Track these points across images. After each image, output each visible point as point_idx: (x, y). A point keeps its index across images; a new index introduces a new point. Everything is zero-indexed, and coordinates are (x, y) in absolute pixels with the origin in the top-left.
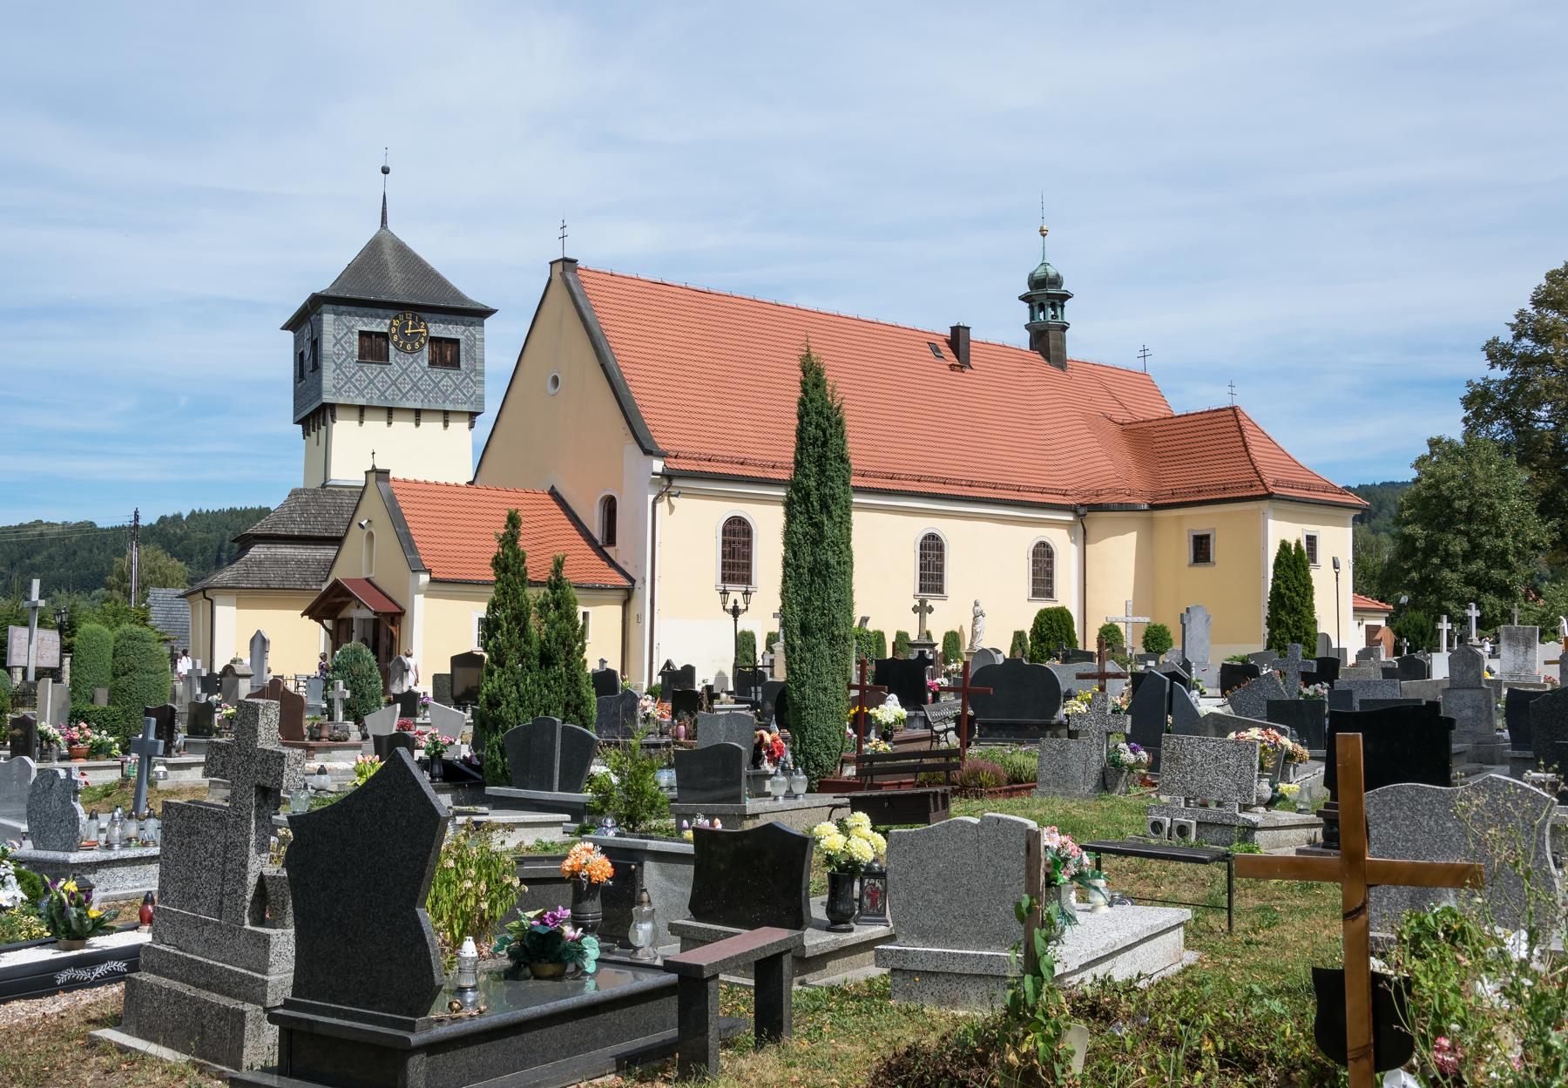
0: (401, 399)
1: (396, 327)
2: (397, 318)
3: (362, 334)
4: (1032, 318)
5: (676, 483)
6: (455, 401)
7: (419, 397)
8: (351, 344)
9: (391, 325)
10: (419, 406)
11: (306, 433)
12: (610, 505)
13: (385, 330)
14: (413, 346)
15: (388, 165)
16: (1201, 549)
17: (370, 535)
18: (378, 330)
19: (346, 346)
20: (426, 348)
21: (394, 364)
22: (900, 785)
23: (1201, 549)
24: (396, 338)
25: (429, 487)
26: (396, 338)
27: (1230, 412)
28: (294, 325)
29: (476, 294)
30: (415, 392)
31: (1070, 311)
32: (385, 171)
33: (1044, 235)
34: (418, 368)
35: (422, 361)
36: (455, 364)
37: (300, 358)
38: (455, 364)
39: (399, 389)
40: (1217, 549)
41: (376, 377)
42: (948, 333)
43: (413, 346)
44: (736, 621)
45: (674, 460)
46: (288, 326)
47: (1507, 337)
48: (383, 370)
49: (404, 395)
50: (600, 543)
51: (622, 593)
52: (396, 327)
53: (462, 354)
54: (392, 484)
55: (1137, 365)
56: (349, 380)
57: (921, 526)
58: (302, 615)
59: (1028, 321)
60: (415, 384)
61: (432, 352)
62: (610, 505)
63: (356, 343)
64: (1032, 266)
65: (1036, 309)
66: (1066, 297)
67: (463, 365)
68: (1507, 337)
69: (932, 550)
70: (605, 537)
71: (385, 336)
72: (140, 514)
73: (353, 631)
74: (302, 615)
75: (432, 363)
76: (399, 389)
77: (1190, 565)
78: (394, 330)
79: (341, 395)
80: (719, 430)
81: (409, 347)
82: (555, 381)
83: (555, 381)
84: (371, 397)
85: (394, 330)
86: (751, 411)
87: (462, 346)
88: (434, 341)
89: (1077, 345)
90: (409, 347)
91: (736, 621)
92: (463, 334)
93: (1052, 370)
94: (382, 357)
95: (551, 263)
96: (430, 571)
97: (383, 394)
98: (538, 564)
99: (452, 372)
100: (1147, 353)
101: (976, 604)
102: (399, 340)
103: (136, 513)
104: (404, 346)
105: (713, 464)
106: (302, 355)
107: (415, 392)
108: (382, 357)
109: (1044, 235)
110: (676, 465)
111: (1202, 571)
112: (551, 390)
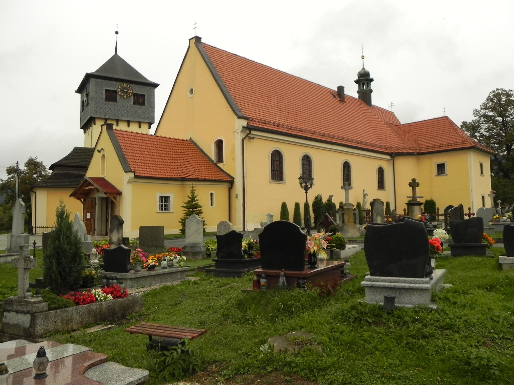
0: (122, 116)
1: (120, 89)
2: (121, 85)
3: (106, 90)
4: (359, 88)
5: (253, 132)
6: (143, 118)
7: (129, 116)
8: (102, 94)
9: (118, 88)
10: (129, 120)
11: (85, 132)
12: (219, 144)
13: (116, 90)
14: (127, 96)
15: (118, 31)
16: (441, 168)
17: (104, 156)
18: (113, 89)
19: (100, 95)
20: (132, 97)
21: (119, 103)
22: (410, 283)
23: (441, 168)
24: (120, 92)
25: (133, 134)
26: (120, 93)
27: (445, 118)
28: (80, 90)
29: (151, 78)
30: (128, 114)
31: (373, 85)
32: (117, 33)
33: (363, 59)
34: (129, 105)
35: (131, 102)
36: (143, 104)
37: (82, 102)
38: (143, 104)
39: (121, 113)
40: (448, 169)
41: (112, 107)
42: (336, 89)
43: (127, 96)
44: (306, 193)
45: (251, 122)
46: (78, 91)
47: (479, 108)
48: (115, 105)
49: (123, 115)
50: (215, 162)
51: (227, 184)
52: (120, 89)
53: (146, 100)
54: (115, 131)
55: (389, 109)
56: (101, 108)
57: (344, 158)
58: (70, 196)
59: (358, 90)
60: (128, 111)
61: (134, 99)
62: (219, 144)
63: (104, 94)
64: (359, 69)
65: (361, 85)
66: (372, 80)
67: (146, 105)
68: (479, 108)
69: (346, 167)
70: (217, 159)
71: (116, 92)
72: (19, 163)
73: (96, 204)
74: (70, 196)
75: (134, 103)
76: (121, 113)
77: (436, 176)
78: (119, 90)
79: (98, 114)
80: (267, 112)
81: (125, 97)
82: (192, 91)
83: (192, 91)
84: (110, 115)
85: (119, 90)
86: (277, 106)
87: (146, 97)
88: (135, 95)
89: (376, 100)
90: (125, 97)
91: (306, 193)
92: (146, 93)
93: (368, 107)
94: (115, 100)
95: (190, 40)
96: (134, 172)
97: (115, 114)
98: (188, 170)
99: (142, 107)
100: (393, 105)
101: (364, 191)
102: (121, 94)
103: (17, 163)
104: (123, 96)
105: (267, 125)
106: (83, 101)
107: (128, 114)
108: (115, 100)
109: (363, 59)
110: (253, 124)
111: (441, 178)
112: (190, 95)
